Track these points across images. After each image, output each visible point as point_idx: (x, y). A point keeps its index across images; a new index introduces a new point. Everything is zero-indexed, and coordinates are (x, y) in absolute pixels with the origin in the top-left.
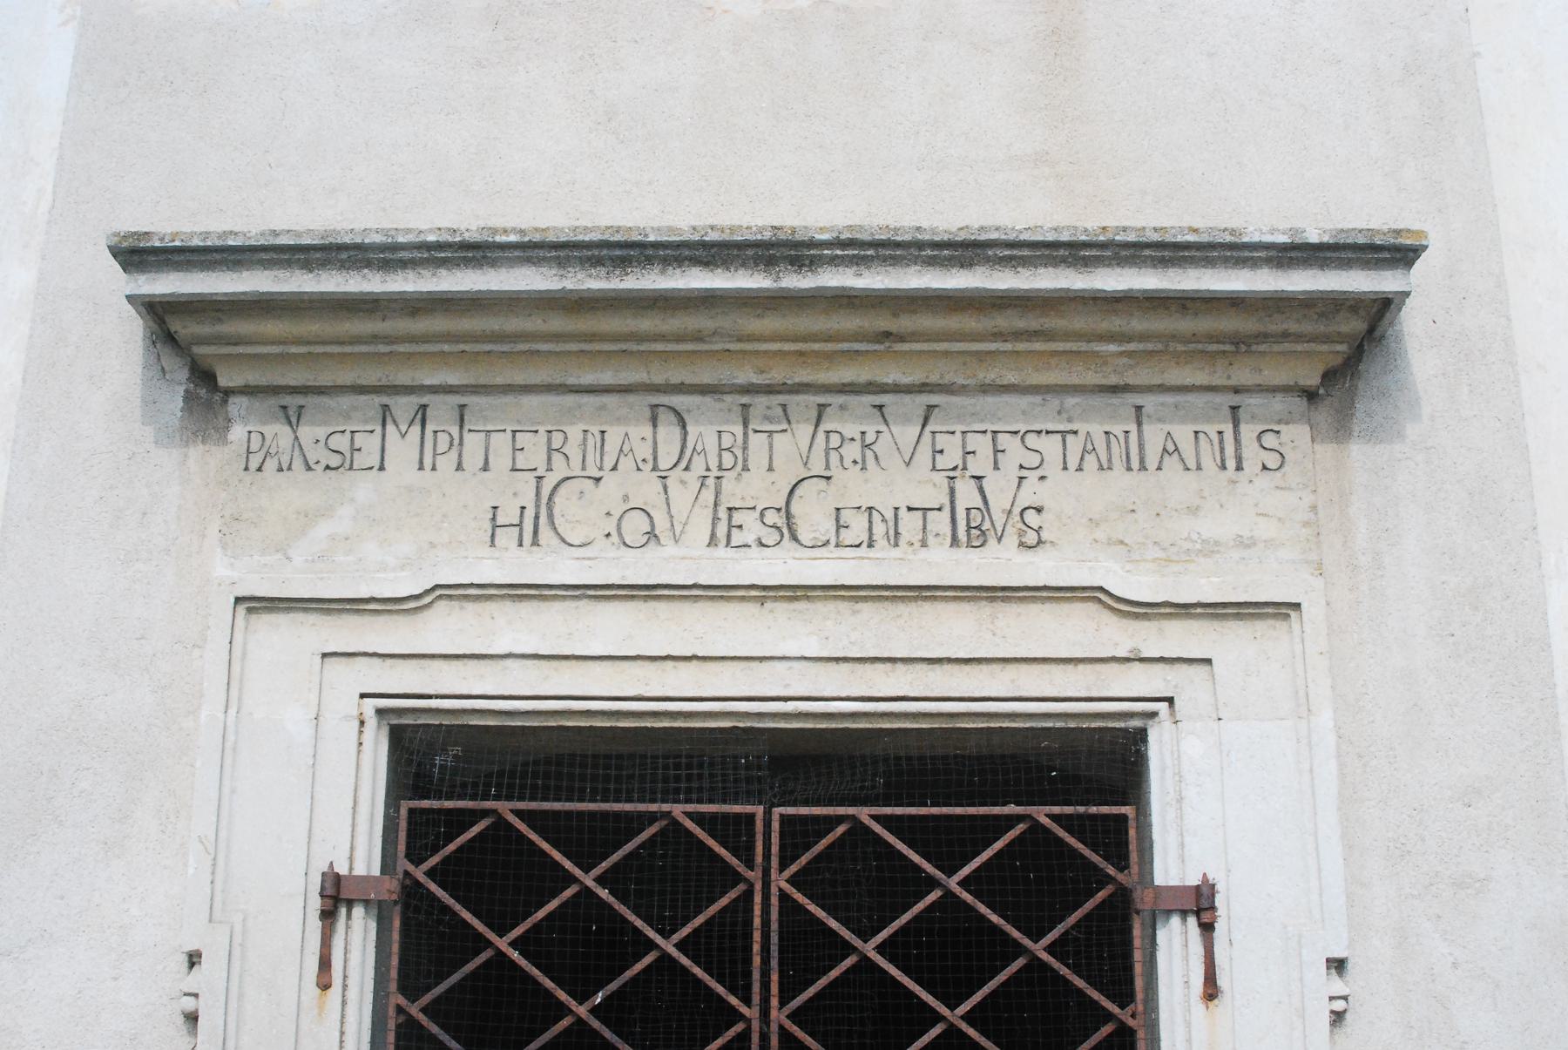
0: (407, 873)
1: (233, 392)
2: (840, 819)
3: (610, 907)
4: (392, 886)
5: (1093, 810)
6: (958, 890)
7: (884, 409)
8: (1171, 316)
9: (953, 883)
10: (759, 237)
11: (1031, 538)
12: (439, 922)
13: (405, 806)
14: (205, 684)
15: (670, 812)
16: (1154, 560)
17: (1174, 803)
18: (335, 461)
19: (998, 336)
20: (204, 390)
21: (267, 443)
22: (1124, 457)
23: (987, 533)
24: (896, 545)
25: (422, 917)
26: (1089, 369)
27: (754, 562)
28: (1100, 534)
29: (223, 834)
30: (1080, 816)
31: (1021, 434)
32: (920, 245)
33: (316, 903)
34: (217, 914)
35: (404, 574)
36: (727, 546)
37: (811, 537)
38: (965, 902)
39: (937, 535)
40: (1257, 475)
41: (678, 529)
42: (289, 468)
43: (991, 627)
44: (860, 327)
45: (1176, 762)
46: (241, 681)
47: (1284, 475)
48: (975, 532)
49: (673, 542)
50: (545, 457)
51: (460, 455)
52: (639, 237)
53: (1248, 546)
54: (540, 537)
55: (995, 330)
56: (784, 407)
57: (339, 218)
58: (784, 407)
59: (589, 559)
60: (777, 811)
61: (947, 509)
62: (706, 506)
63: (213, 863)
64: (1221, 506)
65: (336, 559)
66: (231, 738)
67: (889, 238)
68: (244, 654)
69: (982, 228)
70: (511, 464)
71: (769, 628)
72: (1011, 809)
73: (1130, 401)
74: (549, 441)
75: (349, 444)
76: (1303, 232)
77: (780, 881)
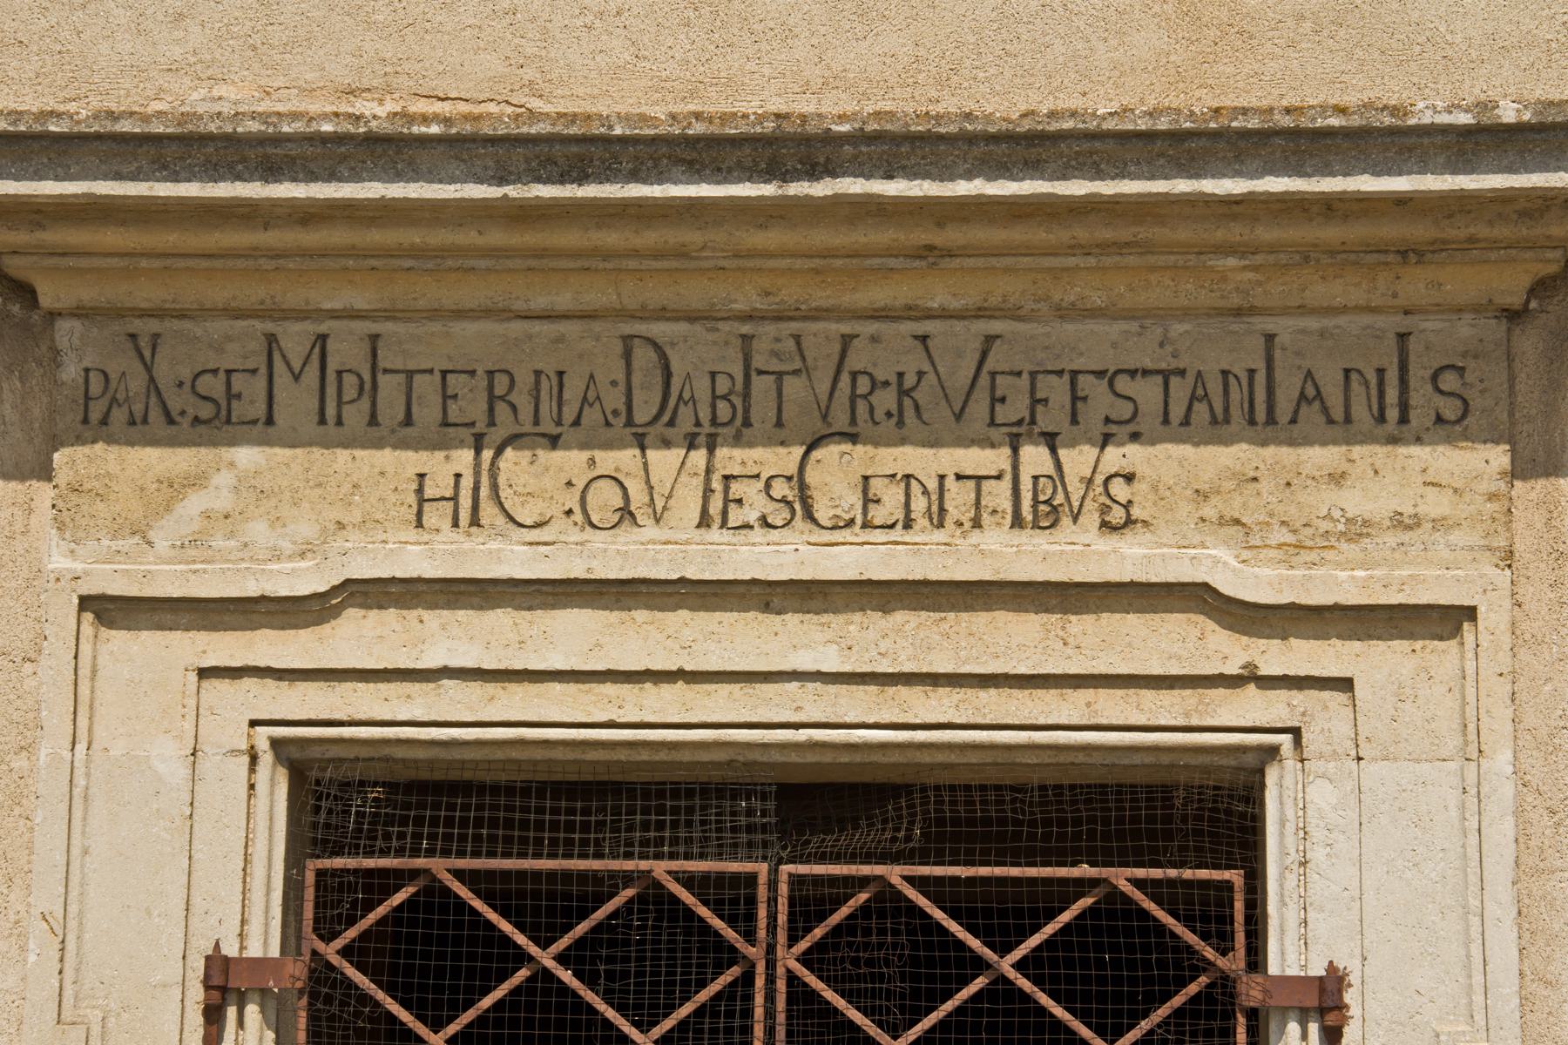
0: (314, 953)
1: (60, 314)
2: (864, 882)
3: (575, 994)
4: (298, 970)
5: (1188, 874)
6: (1012, 974)
7: (928, 340)
8: (1311, 220)
9: (1006, 965)
10: (758, 129)
11: (1117, 515)
12: (357, 1014)
13: (313, 865)
14: (44, 713)
15: (649, 872)
16: (1280, 546)
17: (1295, 867)
18: (206, 411)
19: (1074, 248)
20: (18, 306)
21: (113, 385)
22: (1246, 406)
23: (1060, 509)
24: (941, 525)
25: (335, 1009)
26: (1202, 287)
27: (757, 549)
28: (1209, 511)
29: (73, 909)
30: (1171, 882)
31: (1109, 374)
32: (971, 139)
33: (197, 993)
34: (67, 1014)
35: (303, 564)
36: (721, 527)
37: (830, 515)
38: (1021, 990)
39: (994, 512)
40: (1428, 429)
41: (659, 504)
42: (145, 421)
43: (1061, 633)
44: (894, 240)
45: (1301, 813)
46: (91, 707)
47: (1466, 429)
48: (1042, 507)
49: (652, 521)
50: (485, 406)
51: (374, 404)
52: (602, 130)
53: (1409, 528)
54: (481, 514)
55: (1073, 242)
56: (797, 339)
57: (192, 60)
58: (797, 339)
59: (546, 544)
60: (786, 868)
61: (1008, 477)
62: (695, 474)
63: (60, 947)
64: (1376, 472)
65: (213, 544)
66: (80, 781)
67: (929, 130)
68: (94, 672)
69: (1052, 115)
70: (441, 416)
71: (776, 634)
72: (1085, 870)
73: (1259, 327)
74: (491, 387)
75: (224, 388)
76: (1494, 108)
77: (789, 960)
